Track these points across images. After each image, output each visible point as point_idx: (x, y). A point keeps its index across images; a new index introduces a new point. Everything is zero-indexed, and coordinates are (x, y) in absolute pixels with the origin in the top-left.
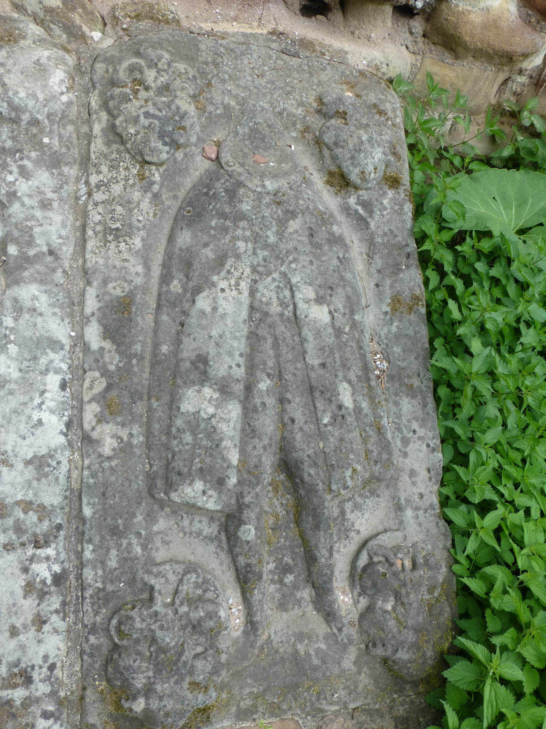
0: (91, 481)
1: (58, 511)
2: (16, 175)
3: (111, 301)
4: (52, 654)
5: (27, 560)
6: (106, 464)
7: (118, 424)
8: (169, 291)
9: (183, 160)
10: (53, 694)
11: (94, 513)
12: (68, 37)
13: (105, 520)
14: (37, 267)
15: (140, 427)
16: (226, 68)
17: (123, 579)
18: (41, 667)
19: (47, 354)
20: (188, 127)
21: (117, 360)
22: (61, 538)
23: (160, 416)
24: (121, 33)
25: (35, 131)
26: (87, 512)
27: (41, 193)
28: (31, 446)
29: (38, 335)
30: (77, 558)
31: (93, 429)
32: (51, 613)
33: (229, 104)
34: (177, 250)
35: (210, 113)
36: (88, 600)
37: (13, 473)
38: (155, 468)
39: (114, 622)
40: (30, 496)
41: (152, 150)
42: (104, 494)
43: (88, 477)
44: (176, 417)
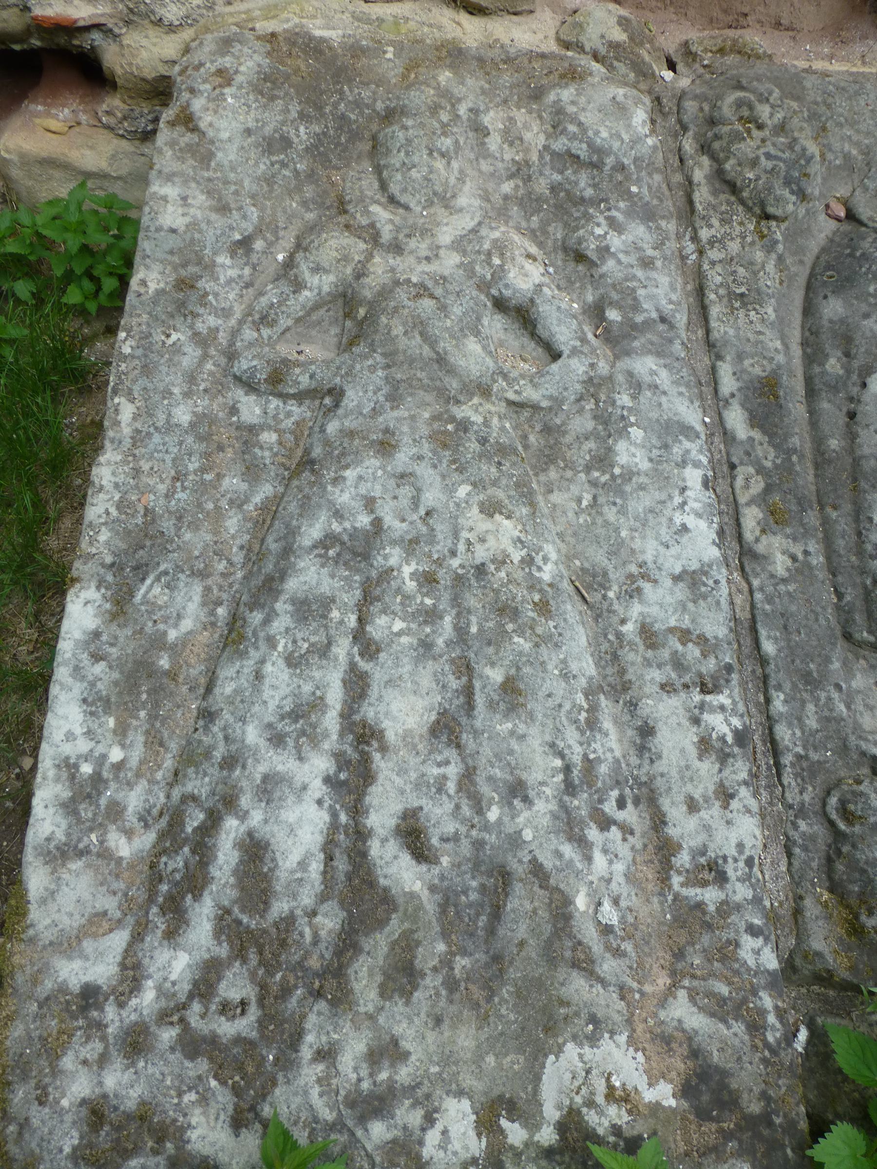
0: (767, 607)
1: (726, 646)
2: (606, 229)
3: (751, 381)
4: (749, 843)
5: (695, 707)
6: (782, 588)
7: (788, 537)
8: (824, 373)
9: (804, 217)
10: (757, 900)
11: (779, 651)
12: (637, 76)
13: (793, 661)
14: (649, 336)
15: (818, 543)
16: (840, 110)
17: (829, 746)
18: (736, 860)
19: (680, 442)
20: (812, 174)
21: (773, 455)
22: (734, 682)
23: (844, 530)
24: (701, 70)
25: (620, 178)
26: (769, 647)
27: (639, 249)
28: (678, 557)
29: (666, 417)
30: (761, 712)
31: (757, 540)
32: (739, 785)
33: (850, 152)
34: (825, 323)
35: (830, 163)
36: (789, 769)
37: (660, 591)
38: (848, 598)
39: (833, 801)
40: (686, 623)
41: (777, 200)
42: (785, 627)
43: (762, 602)
44: (868, 530)
